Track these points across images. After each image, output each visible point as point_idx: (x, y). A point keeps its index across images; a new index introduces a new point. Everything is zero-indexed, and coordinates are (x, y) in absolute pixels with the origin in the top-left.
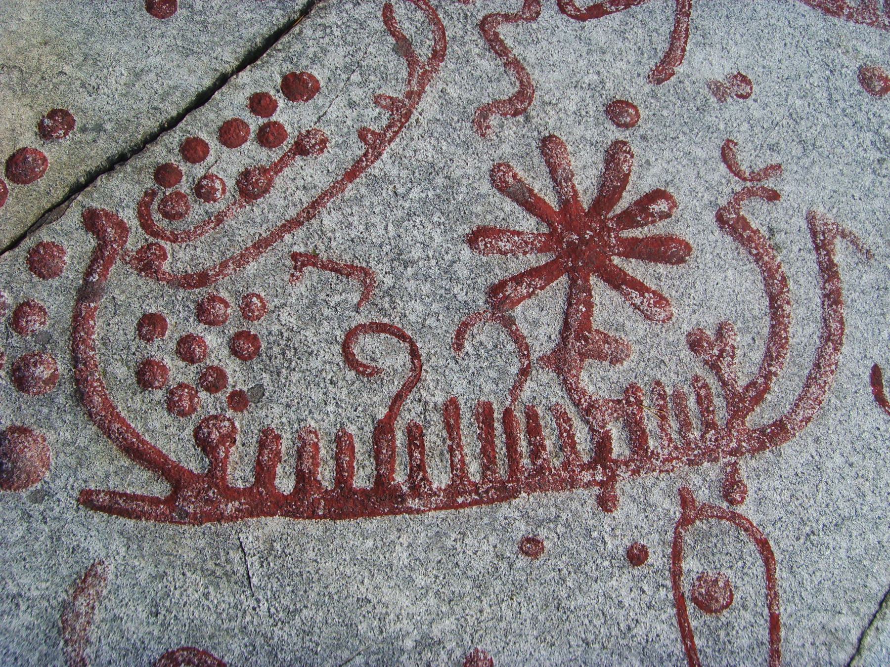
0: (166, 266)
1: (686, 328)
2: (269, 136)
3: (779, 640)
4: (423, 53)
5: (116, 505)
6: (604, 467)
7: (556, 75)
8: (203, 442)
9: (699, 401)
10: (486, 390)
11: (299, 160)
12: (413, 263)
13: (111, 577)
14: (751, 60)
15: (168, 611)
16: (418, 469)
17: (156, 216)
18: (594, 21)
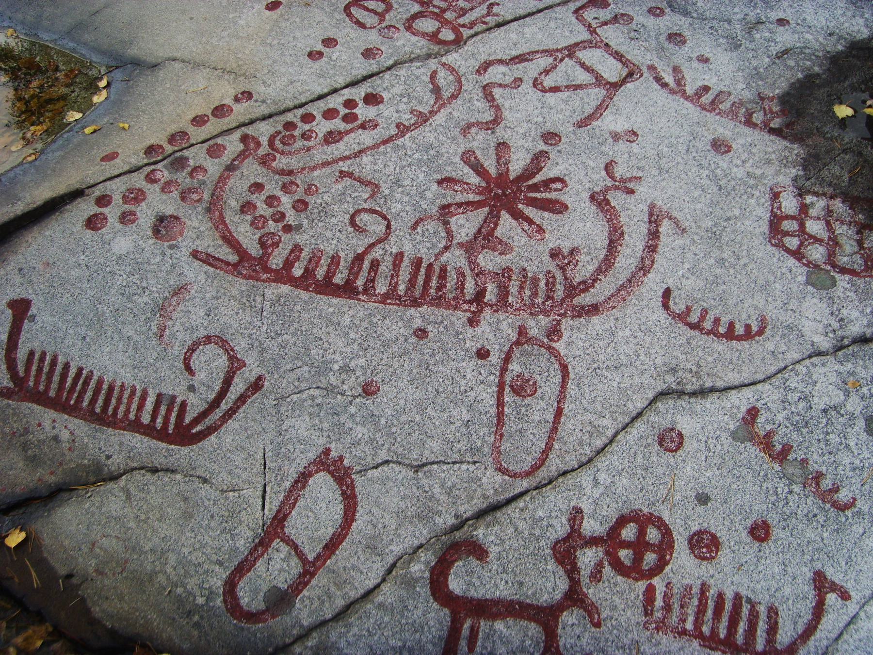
0: (274, 164)
1: (551, 245)
2: (349, 118)
3: (559, 423)
4: (446, 94)
5: (209, 260)
6: (478, 305)
7: (519, 115)
8: (262, 244)
9: (547, 284)
10: (422, 252)
11: (360, 131)
12: (403, 186)
13: (193, 292)
14: (643, 125)
15: (215, 316)
16: (371, 281)
17: (277, 142)
18: (552, 94)
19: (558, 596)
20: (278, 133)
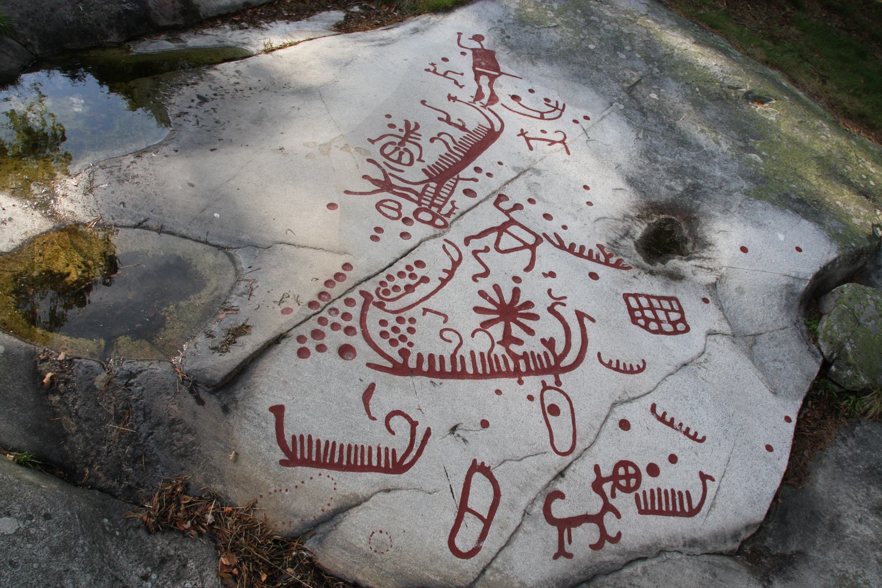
2: (413, 276)
19: (600, 508)
20: (379, 289)
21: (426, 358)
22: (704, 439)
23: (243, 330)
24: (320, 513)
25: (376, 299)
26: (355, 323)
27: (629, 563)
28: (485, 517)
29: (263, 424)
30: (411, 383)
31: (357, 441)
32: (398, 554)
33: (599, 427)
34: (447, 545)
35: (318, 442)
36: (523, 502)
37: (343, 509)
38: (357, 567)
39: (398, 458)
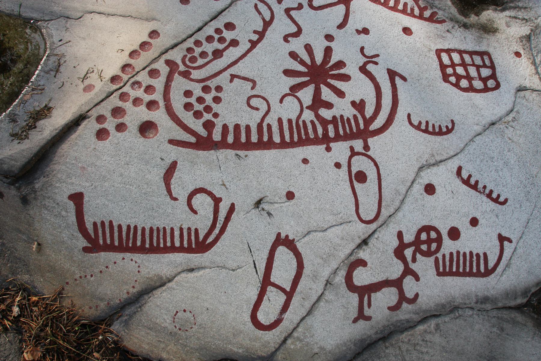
2: (222, 40)
19: (400, 273)
20: (185, 56)
21: (231, 129)
22: (506, 200)
23: (45, 112)
24: (125, 296)
25: (182, 68)
26: (158, 96)
27: (424, 320)
28: (288, 289)
29: (64, 213)
30: (215, 158)
31: (159, 223)
32: (202, 331)
33: (404, 192)
34: (250, 320)
35: (120, 227)
36: (326, 273)
37: (137, 299)
38: (162, 346)
39: (201, 238)
